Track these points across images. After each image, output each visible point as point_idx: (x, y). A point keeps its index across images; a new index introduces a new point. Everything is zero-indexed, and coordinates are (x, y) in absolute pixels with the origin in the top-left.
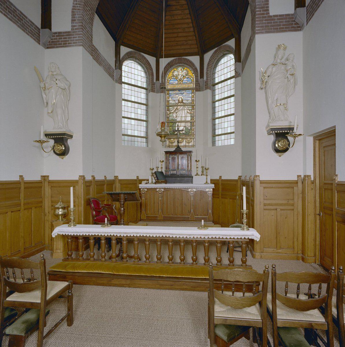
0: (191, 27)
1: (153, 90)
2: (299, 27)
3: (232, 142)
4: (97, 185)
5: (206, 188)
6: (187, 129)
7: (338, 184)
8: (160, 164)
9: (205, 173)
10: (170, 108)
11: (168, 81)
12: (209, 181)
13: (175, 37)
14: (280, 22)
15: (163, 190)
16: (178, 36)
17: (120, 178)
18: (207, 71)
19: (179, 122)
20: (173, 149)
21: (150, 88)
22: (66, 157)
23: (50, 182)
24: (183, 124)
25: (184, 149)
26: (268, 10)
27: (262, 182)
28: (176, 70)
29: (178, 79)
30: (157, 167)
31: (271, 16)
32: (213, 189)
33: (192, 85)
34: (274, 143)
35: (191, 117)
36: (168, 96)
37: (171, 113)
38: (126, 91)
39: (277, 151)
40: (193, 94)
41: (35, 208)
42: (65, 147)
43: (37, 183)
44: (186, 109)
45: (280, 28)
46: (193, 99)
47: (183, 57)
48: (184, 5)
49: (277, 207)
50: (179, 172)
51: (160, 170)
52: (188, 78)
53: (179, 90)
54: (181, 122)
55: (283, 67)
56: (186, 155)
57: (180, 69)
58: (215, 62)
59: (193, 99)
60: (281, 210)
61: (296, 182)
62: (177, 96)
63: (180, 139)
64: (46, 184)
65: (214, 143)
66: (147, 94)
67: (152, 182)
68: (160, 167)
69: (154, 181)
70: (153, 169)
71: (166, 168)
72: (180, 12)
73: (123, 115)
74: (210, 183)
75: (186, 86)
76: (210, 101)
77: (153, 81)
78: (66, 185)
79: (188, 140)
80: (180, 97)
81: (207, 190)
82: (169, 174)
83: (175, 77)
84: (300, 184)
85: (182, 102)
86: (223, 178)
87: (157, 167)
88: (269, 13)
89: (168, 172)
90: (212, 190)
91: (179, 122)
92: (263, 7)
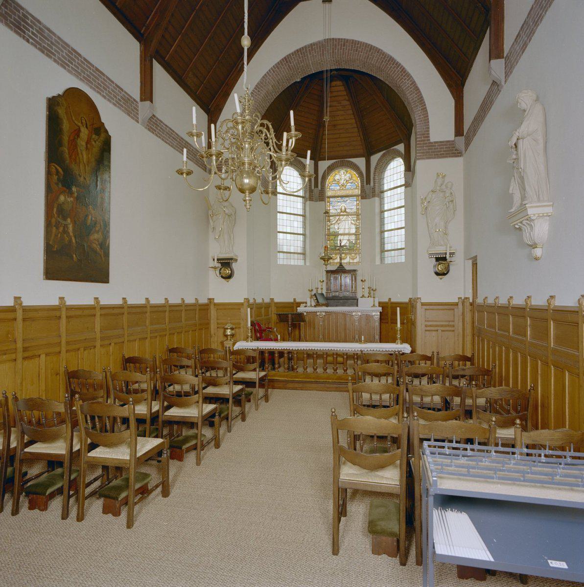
0: (354, 128)
1: (311, 199)
2: (460, 153)
3: (403, 259)
4: (277, 307)
5: (373, 311)
6: (351, 242)
7: (555, 310)
8: (320, 284)
9: (372, 294)
10: (331, 218)
11: (328, 187)
12: (377, 304)
13: (336, 138)
14: (441, 148)
15: (324, 314)
16: (339, 138)
17: (276, 300)
18: (375, 175)
19: (341, 235)
20: (334, 268)
21: (308, 196)
22: (231, 280)
23: (215, 304)
24: (346, 237)
25: (347, 268)
26: (429, 137)
27: (423, 304)
28: (337, 173)
29: (340, 184)
30: (316, 288)
31: (432, 143)
32: (380, 312)
33: (357, 190)
34: (435, 266)
35: (357, 228)
36: (328, 204)
37: (332, 224)
38: (283, 203)
39: (437, 274)
40: (358, 202)
41: (205, 329)
42: (231, 270)
43: (117, 308)
44: (349, 219)
45: (440, 154)
46: (358, 207)
47: (345, 159)
48: (346, 105)
49: (439, 328)
50: (342, 294)
51: (320, 292)
52: (353, 182)
53: (342, 197)
54: (344, 234)
55: (441, 195)
56: (350, 275)
57: (342, 172)
58: (382, 166)
59: (358, 207)
60: (442, 331)
61: (457, 304)
62: (339, 204)
63: (343, 255)
64: (212, 307)
65: (382, 259)
66: (304, 204)
67: (311, 305)
68: (320, 288)
69: (313, 304)
70: (312, 290)
71: (327, 289)
72: (342, 112)
73: (278, 230)
74: (378, 306)
75: (350, 193)
76: (377, 210)
77: (311, 188)
78: (235, 307)
79: (353, 256)
80: (343, 205)
81: (374, 314)
82: (331, 296)
83: (336, 182)
84: (460, 306)
85: (345, 211)
86: (392, 301)
87: (316, 288)
88: (429, 140)
89: (330, 294)
90: (379, 313)
91: (341, 235)
92: (424, 134)
